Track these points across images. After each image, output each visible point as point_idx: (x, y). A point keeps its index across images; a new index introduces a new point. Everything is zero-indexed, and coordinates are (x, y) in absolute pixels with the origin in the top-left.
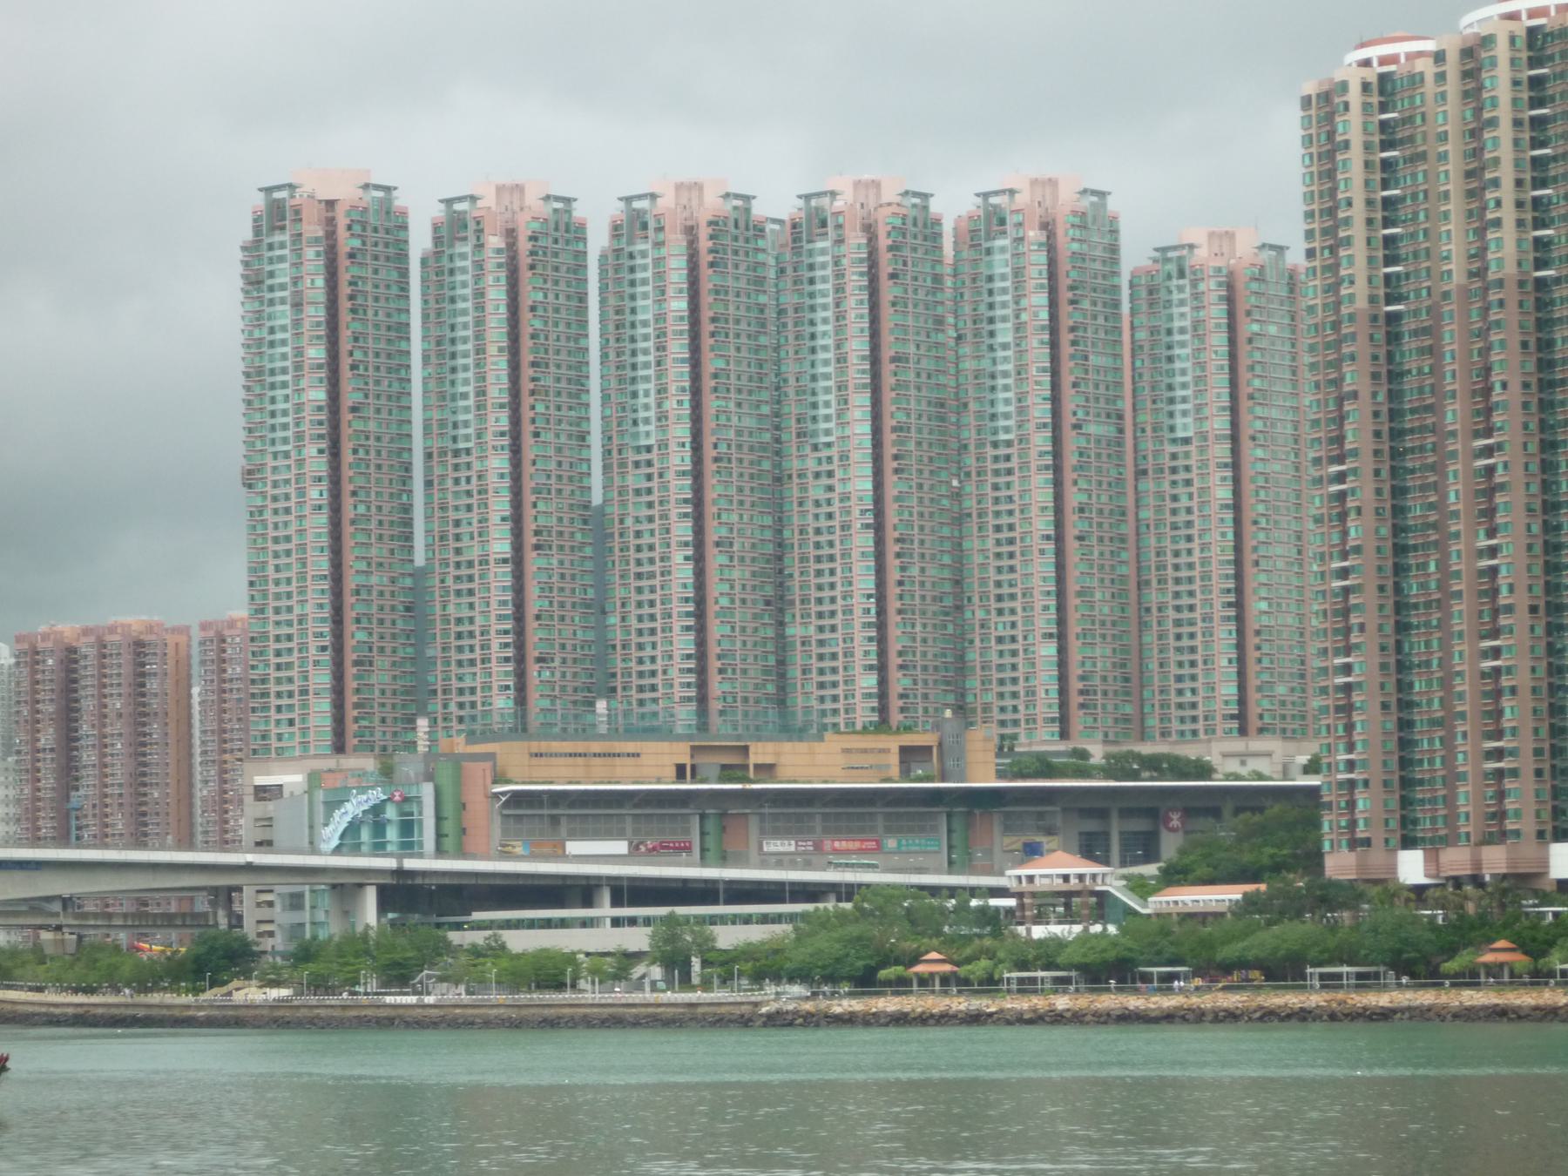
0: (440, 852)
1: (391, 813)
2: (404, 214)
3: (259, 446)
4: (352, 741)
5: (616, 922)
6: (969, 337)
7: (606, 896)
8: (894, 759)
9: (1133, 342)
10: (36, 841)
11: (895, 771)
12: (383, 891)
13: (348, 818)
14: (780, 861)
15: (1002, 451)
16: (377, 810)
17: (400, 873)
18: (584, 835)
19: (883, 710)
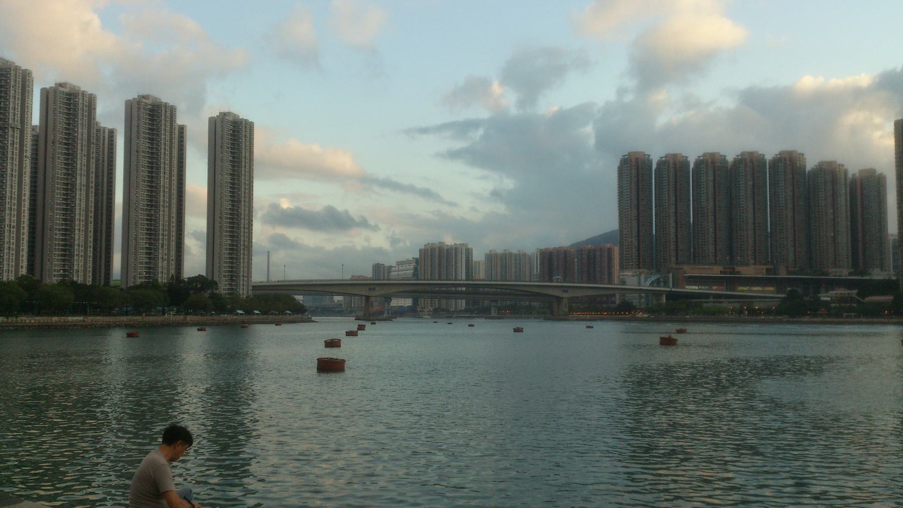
0: (673, 287)
1: (661, 279)
2: (652, 160)
3: (622, 207)
4: (641, 266)
5: (714, 302)
6: (185, 393)
7: (712, 297)
8: (764, 271)
9: (500, 281)
10: (544, 281)
11: (765, 273)
12: (666, 295)
13: (651, 281)
14: (715, 290)
15: (780, 208)
16: (658, 279)
17: (671, 291)
18: (741, 286)
19: (531, 278)
